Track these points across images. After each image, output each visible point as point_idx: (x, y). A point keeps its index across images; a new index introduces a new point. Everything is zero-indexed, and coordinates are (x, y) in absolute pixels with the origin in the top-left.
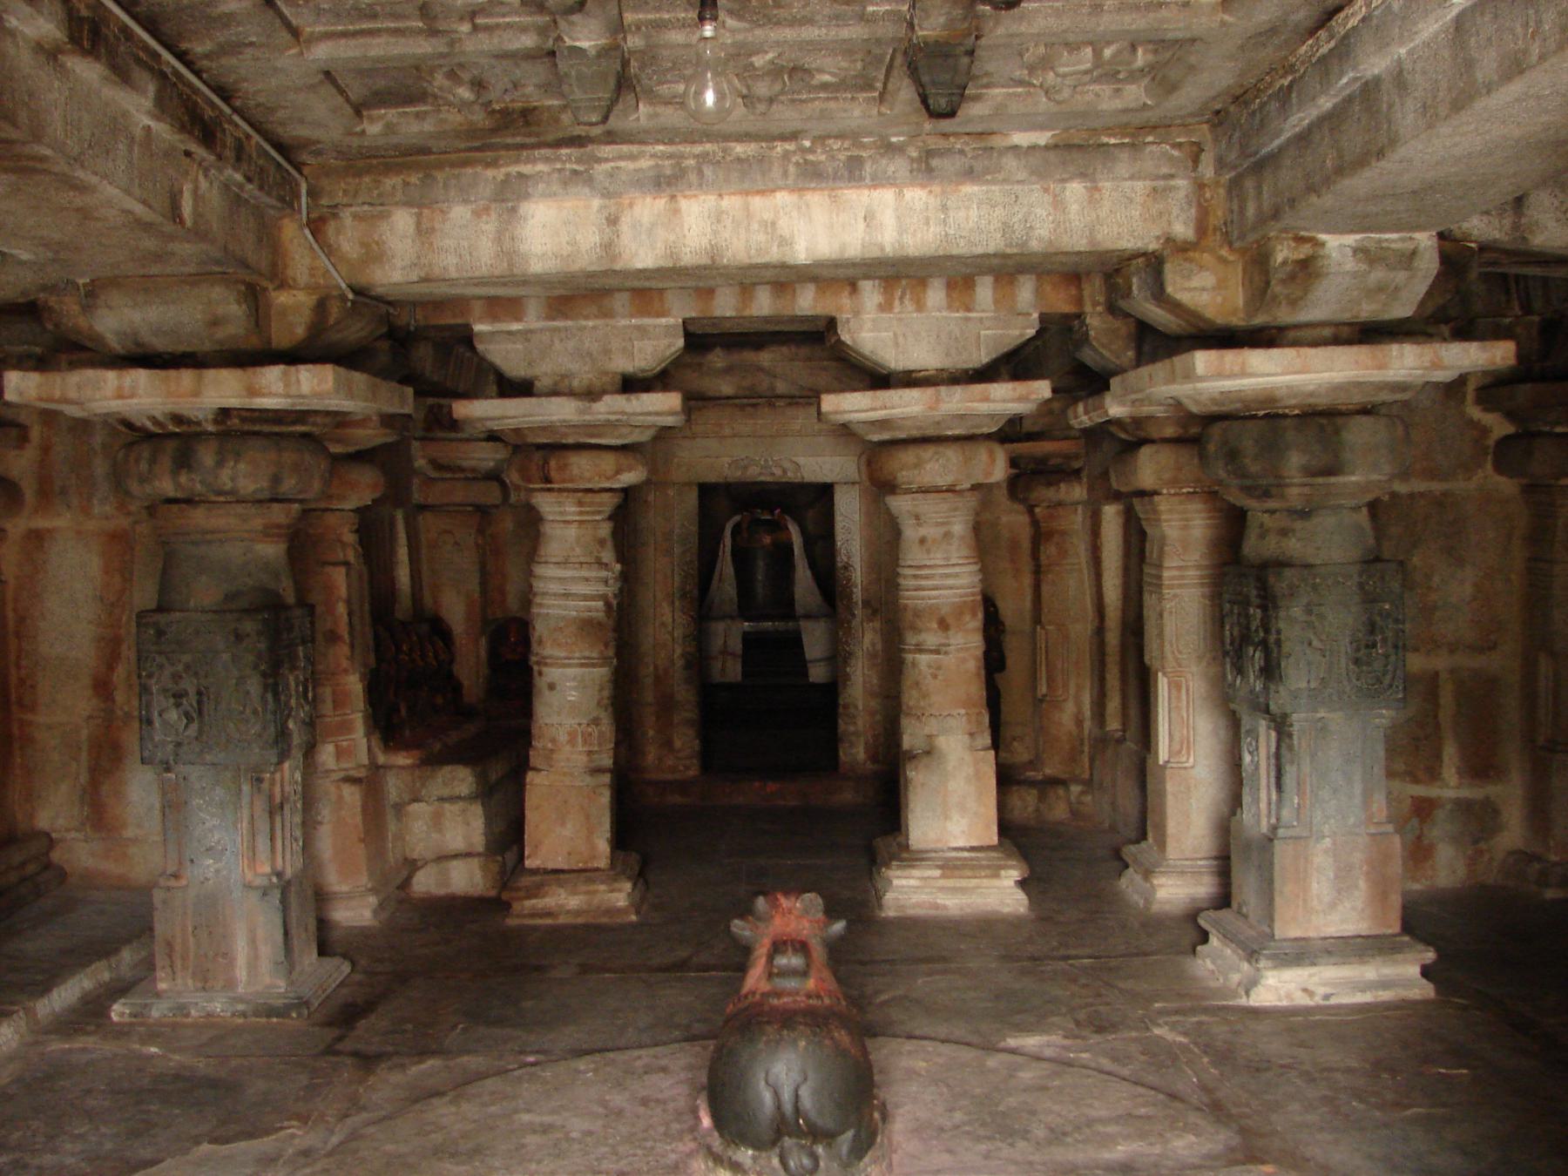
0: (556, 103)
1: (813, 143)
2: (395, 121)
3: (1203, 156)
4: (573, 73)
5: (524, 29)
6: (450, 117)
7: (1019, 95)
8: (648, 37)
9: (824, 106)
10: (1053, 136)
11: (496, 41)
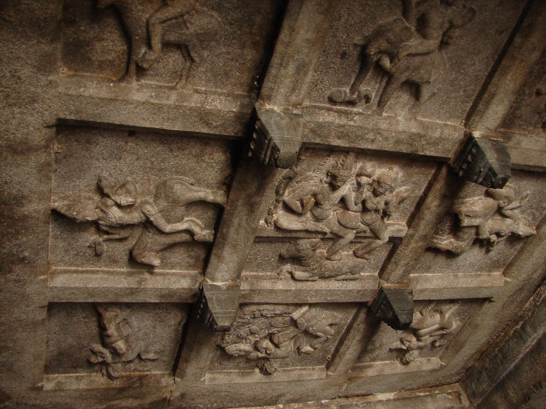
0: (158, 372)
1: (284, 405)
2: (63, 381)
3: (461, 397)
4: (214, 298)
5: (184, 276)
6: (97, 379)
7: (388, 364)
8: (252, 284)
9: (300, 372)
10: (395, 394)
11: (166, 281)
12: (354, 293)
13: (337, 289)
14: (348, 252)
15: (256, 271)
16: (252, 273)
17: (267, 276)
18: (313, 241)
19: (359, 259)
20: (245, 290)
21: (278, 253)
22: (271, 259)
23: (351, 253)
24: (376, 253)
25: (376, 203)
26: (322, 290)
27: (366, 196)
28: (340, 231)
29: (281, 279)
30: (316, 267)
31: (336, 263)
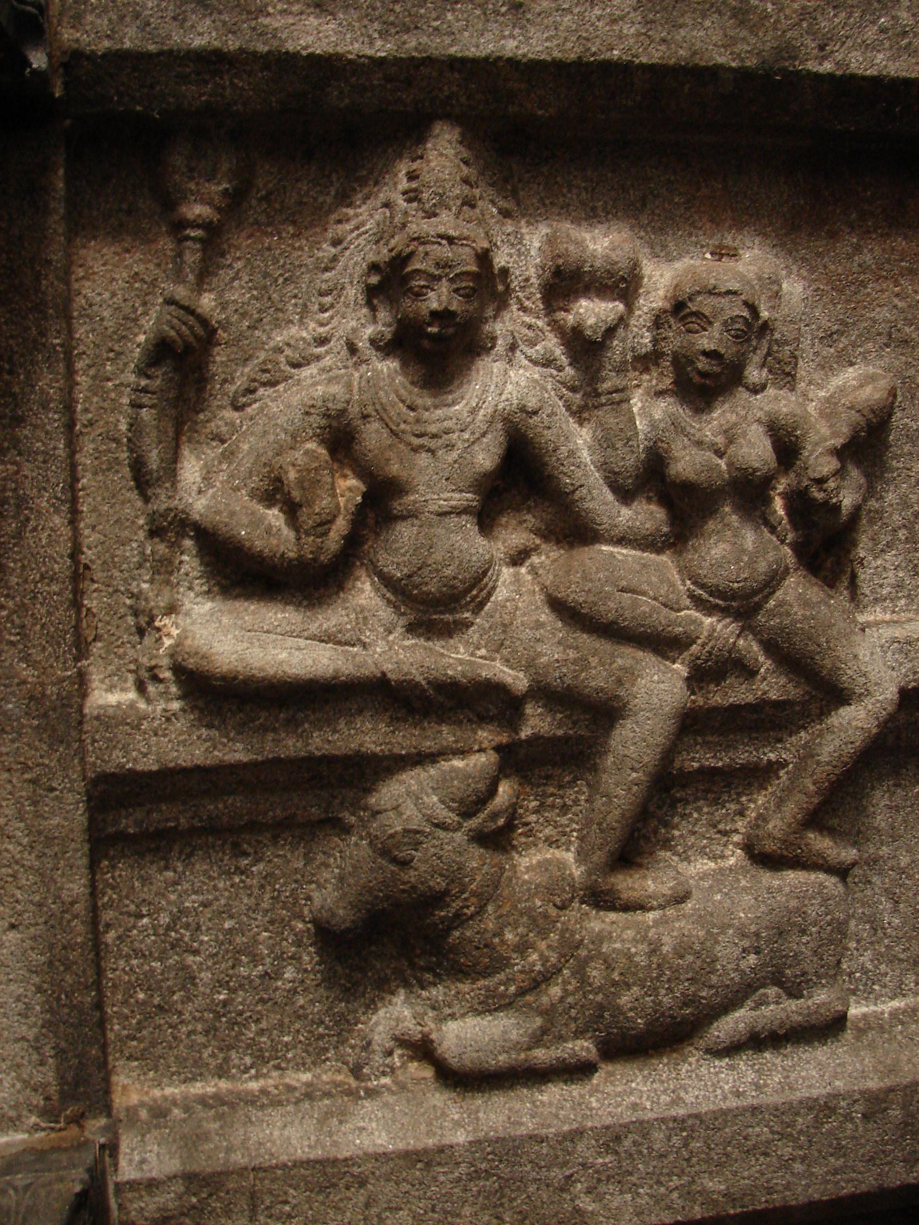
12: (848, 1117)
13: (733, 1103)
14: (714, 858)
15: (222, 1072)
16: (197, 1088)
17: (290, 1089)
18: (454, 769)
19: (792, 877)
20: (152, 1185)
21: (301, 917)
22: (278, 974)
23: (735, 858)
24: (885, 850)
25: (720, 440)
26: (643, 1128)
27: (653, 425)
28: (583, 663)
29: (372, 1093)
30: (544, 959)
31: (663, 921)
